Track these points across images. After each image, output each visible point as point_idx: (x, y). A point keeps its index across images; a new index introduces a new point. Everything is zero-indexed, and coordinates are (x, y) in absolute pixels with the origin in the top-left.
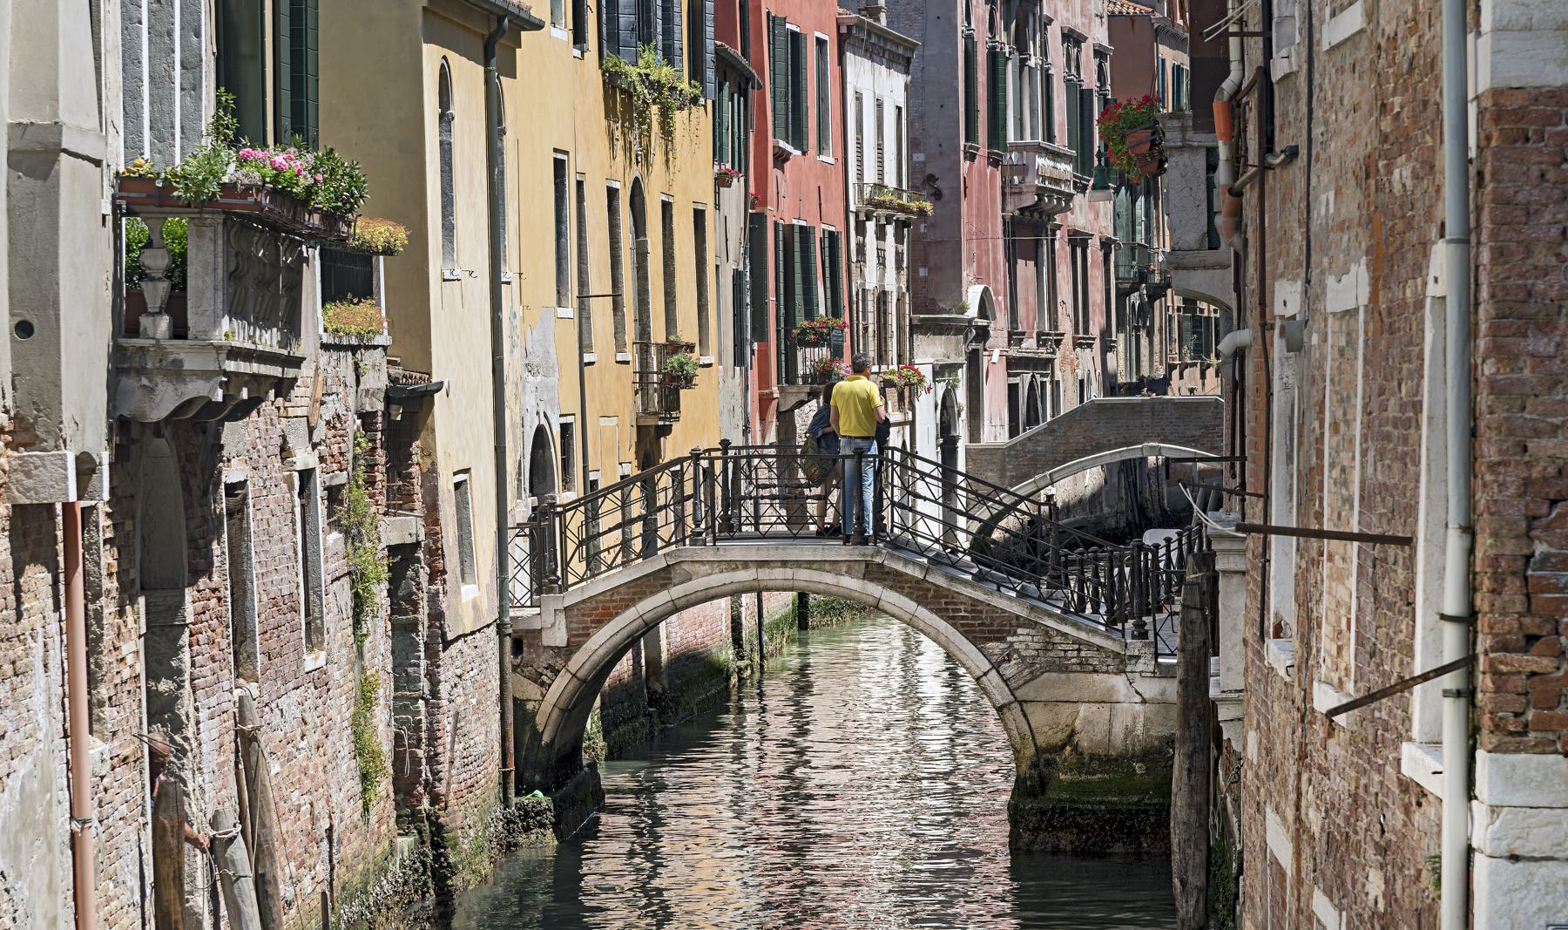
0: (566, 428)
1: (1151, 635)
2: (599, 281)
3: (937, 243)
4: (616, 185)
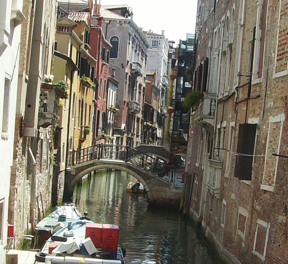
0: (71, 139)
1: (174, 182)
2: (77, 116)
3: (118, 116)
4: (80, 99)
